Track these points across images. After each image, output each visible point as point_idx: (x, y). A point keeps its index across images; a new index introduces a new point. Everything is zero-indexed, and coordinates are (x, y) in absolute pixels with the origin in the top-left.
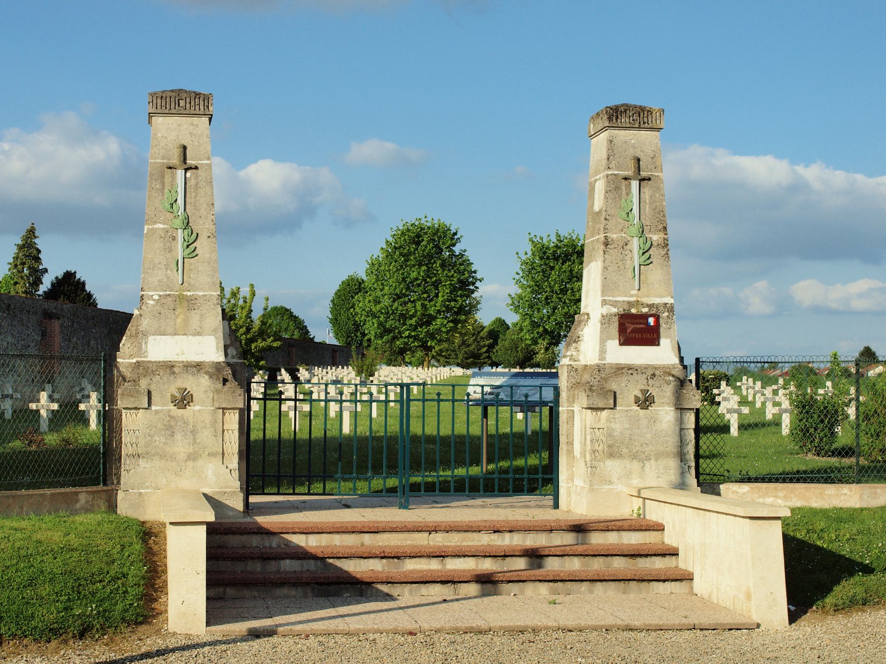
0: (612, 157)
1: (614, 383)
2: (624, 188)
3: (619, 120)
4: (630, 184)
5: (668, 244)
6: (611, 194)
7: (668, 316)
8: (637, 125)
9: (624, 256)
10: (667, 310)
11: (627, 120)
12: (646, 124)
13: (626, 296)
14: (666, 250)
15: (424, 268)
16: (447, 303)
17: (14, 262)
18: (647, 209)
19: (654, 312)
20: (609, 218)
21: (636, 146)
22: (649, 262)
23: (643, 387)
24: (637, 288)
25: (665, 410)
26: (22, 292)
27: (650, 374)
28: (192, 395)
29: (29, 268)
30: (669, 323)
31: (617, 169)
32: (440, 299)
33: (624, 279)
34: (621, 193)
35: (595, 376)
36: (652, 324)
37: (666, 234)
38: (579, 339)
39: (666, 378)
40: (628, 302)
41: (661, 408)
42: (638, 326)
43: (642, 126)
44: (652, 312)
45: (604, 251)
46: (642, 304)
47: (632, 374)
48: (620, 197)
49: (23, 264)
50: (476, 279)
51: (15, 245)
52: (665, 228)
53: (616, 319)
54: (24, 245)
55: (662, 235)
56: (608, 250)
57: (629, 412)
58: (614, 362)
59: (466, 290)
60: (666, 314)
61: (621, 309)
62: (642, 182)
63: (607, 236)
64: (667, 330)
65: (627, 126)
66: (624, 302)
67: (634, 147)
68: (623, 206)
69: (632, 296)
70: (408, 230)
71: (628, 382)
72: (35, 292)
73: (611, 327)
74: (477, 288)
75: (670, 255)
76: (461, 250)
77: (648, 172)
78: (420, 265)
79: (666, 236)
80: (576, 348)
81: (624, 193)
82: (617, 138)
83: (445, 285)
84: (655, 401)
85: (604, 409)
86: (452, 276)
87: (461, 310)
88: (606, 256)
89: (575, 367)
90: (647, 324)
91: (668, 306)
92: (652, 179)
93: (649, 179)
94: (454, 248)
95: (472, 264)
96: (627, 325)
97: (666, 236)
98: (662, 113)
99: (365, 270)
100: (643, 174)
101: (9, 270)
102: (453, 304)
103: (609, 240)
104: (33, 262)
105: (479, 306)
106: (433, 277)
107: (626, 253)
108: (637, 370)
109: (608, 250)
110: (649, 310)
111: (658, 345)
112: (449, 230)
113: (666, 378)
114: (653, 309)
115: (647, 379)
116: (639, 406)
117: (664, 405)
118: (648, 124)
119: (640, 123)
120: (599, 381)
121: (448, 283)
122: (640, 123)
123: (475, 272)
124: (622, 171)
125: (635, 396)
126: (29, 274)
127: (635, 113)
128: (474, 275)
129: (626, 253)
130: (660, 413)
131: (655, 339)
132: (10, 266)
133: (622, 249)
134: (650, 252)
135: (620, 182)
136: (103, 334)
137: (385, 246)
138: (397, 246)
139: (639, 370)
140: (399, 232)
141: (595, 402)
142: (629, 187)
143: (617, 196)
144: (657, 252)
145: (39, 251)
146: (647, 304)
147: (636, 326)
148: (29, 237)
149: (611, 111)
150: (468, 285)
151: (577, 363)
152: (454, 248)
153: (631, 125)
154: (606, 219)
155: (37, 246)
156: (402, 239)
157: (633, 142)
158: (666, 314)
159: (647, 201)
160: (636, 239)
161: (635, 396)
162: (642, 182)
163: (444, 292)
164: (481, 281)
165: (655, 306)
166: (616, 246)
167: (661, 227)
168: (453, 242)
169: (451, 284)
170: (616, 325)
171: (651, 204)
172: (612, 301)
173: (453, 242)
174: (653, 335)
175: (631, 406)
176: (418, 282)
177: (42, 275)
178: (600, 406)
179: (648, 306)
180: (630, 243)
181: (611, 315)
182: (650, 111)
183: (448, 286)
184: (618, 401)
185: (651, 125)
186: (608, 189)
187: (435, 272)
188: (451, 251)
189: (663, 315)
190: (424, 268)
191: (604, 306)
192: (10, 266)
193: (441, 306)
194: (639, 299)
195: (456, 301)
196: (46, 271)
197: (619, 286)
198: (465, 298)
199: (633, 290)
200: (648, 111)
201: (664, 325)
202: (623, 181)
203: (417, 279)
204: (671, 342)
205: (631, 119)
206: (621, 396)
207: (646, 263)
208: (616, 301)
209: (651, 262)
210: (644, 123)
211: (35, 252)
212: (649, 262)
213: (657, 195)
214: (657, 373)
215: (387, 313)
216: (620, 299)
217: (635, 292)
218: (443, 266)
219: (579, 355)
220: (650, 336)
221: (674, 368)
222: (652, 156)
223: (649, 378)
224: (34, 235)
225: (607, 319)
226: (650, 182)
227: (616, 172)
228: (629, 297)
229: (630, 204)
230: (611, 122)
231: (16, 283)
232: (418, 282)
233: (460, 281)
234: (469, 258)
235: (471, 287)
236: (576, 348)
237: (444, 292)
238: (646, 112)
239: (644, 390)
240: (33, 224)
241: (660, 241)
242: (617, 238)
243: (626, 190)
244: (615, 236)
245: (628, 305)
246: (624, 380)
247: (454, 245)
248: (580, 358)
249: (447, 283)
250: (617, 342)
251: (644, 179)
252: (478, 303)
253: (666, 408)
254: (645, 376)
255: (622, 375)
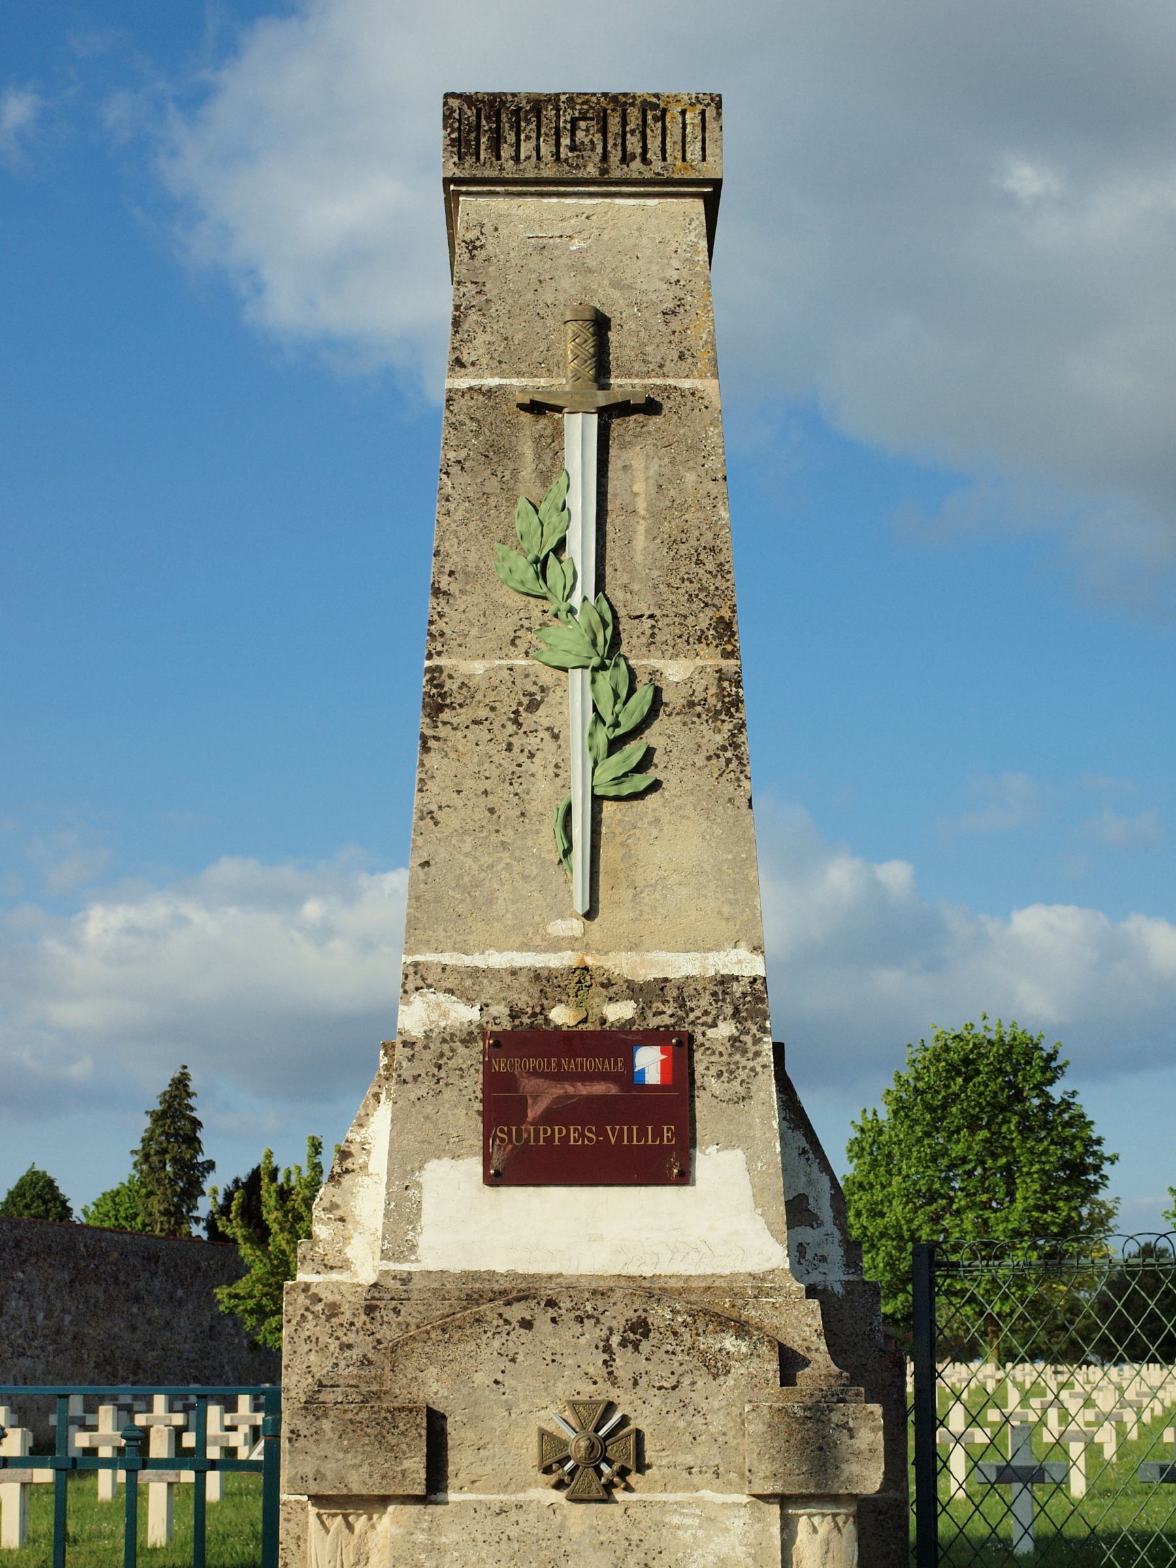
0: (474, 316)
1: (433, 1371)
2: (527, 450)
3: (506, 151)
4: (558, 433)
5: (737, 702)
6: (465, 478)
7: (734, 1040)
8: (592, 171)
9: (523, 758)
10: (729, 1010)
11: (546, 150)
12: (636, 164)
13: (523, 947)
14: (727, 726)
15: (983, 1134)
16: (1035, 1214)
17: (144, 1148)
18: (640, 541)
19: (666, 1020)
20: (454, 588)
21: (592, 263)
22: (640, 782)
23: (587, 1390)
24: (580, 904)
25: (700, 1503)
26: (159, 1211)
27: (619, 1324)
28: (639, 1434)
29: (174, 1161)
30: (743, 1074)
31: (499, 365)
32: (1019, 1205)
33: (517, 868)
34: (515, 472)
35: (351, 1338)
36: (653, 1077)
37: (726, 655)
38: (348, 1164)
39: (703, 1342)
40: (537, 976)
41: (680, 1496)
42: (584, 1090)
43: (616, 174)
44: (653, 1022)
45: (424, 739)
46: (607, 985)
47: (527, 1324)
48: (509, 492)
49: (164, 1151)
50: (1102, 1158)
51: (147, 1113)
52: (725, 628)
53: (470, 1057)
54: (164, 1112)
55: (711, 659)
56: (443, 731)
57: (514, 1515)
58: (457, 1265)
59: (1079, 1184)
60: (726, 1029)
61: (500, 1010)
62: (615, 422)
63: (439, 669)
64: (732, 1108)
65: (547, 173)
66: (514, 972)
67: (580, 267)
68: (519, 526)
69: (555, 945)
70: (947, 1049)
71: (504, 1363)
72: (188, 1212)
73: (447, 1094)
74: (1103, 1177)
75: (746, 749)
76: (1065, 1093)
77: (648, 375)
78: (973, 1127)
79: (729, 665)
80: (334, 1207)
81: (528, 471)
82: (503, 231)
83: (1029, 1174)
84: (650, 1456)
85: (384, 1501)
86: (1045, 1152)
87: (1069, 1228)
88: (433, 760)
89: (328, 1297)
90: (629, 1077)
91: (737, 989)
92: (667, 405)
93: (651, 407)
94: (1048, 1089)
95: (1092, 1123)
96: (528, 1085)
97: (729, 665)
98: (710, 113)
99: (847, 1144)
100: (623, 385)
101: (135, 1165)
102: (1048, 1216)
103: (449, 685)
104: (184, 1147)
105: (1112, 1222)
106: (1000, 1156)
107: (532, 742)
108: (551, 1303)
109: (443, 731)
110: (642, 1014)
111: (684, 1178)
112: (1037, 1047)
113: (703, 1342)
114: (657, 1005)
115: (607, 1349)
116: (559, 1485)
117: (697, 1479)
118: (645, 161)
119: (605, 157)
120: (365, 1362)
121: (1036, 1167)
122: (605, 157)
123: (1099, 1142)
124: (519, 374)
125: (543, 1434)
126: (175, 1174)
127: (584, 118)
128: (1096, 1148)
129: (532, 742)
130: (676, 1520)
131: (664, 1150)
132: (136, 1158)
133: (511, 728)
134: (653, 737)
135: (515, 426)
136: (52, 1285)
137: (893, 1086)
138: (921, 1085)
139: (566, 1304)
140: (928, 1055)
141: (329, 1468)
142: (554, 440)
143: (493, 485)
144: (685, 738)
145: (197, 1124)
146: (630, 984)
147: (570, 1090)
148: (176, 1096)
149: (470, 113)
150: (1085, 1173)
151: (335, 1276)
152: (1048, 1089)
153: (564, 171)
154: (437, 592)
155: (194, 1114)
156: (933, 1069)
157: (575, 245)
158: (726, 1029)
159: (641, 506)
160: (577, 680)
161: (543, 1434)
162: (615, 422)
163: (1027, 1191)
164: (1113, 1163)
165: (671, 993)
166: (483, 713)
167: (704, 620)
168: (1049, 1075)
169: (1042, 1171)
170: (474, 1083)
171: (658, 516)
172: (455, 969)
173: (1049, 1075)
174: (658, 1133)
175: (523, 1488)
176: (968, 1167)
177: (204, 1176)
178: (357, 1488)
179: (634, 990)
180: (552, 698)
181: (448, 1038)
182: (655, 107)
183: (1035, 1176)
184: (458, 1460)
185: (657, 166)
186: (452, 455)
187: (1006, 1143)
188: (1042, 1094)
189: (710, 1033)
190: (983, 1134)
191: (416, 998)
192: (136, 1158)
193: (1021, 1220)
194: (590, 961)
195: (1055, 1209)
196: (210, 1166)
197: (490, 901)
198: (1076, 1202)
199: (562, 916)
200: (646, 106)
201: (713, 1084)
202: (525, 417)
203: (964, 1160)
204: (750, 1161)
205: (565, 141)
206: (469, 1435)
207: (626, 789)
208: (476, 973)
209: (656, 786)
210: (625, 159)
211: (188, 1126)
212: (640, 782)
213: (690, 478)
214: (659, 1315)
215: (900, 1237)
216: (497, 960)
217: (575, 926)
218: (1026, 1130)
219: (346, 1239)
220: (642, 1134)
221: (760, 1292)
222: (669, 305)
223: (615, 1340)
224: (186, 1091)
225: (427, 1055)
226: (657, 420)
227: (493, 382)
228: (537, 949)
229: (554, 520)
230: (470, 160)
231: (150, 1194)
232: (968, 1167)
233: (1066, 1165)
234: (1085, 1110)
235: (1092, 1177)
236: (334, 1207)
237: (1027, 1191)
238: (634, 114)
239: (590, 1404)
240: (185, 1067)
241: (699, 689)
242: (489, 674)
243: (539, 457)
244: (478, 667)
245: (535, 990)
246: (485, 1353)
247: (1051, 1082)
248: (350, 1252)
249: (1034, 1169)
250: (475, 1165)
251: (624, 409)
252: (1110, 1214)
253: (707, 1494)
254: (593, 1333)
255: (477, 1329)
